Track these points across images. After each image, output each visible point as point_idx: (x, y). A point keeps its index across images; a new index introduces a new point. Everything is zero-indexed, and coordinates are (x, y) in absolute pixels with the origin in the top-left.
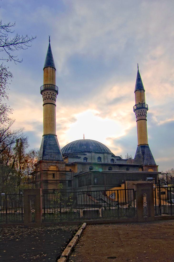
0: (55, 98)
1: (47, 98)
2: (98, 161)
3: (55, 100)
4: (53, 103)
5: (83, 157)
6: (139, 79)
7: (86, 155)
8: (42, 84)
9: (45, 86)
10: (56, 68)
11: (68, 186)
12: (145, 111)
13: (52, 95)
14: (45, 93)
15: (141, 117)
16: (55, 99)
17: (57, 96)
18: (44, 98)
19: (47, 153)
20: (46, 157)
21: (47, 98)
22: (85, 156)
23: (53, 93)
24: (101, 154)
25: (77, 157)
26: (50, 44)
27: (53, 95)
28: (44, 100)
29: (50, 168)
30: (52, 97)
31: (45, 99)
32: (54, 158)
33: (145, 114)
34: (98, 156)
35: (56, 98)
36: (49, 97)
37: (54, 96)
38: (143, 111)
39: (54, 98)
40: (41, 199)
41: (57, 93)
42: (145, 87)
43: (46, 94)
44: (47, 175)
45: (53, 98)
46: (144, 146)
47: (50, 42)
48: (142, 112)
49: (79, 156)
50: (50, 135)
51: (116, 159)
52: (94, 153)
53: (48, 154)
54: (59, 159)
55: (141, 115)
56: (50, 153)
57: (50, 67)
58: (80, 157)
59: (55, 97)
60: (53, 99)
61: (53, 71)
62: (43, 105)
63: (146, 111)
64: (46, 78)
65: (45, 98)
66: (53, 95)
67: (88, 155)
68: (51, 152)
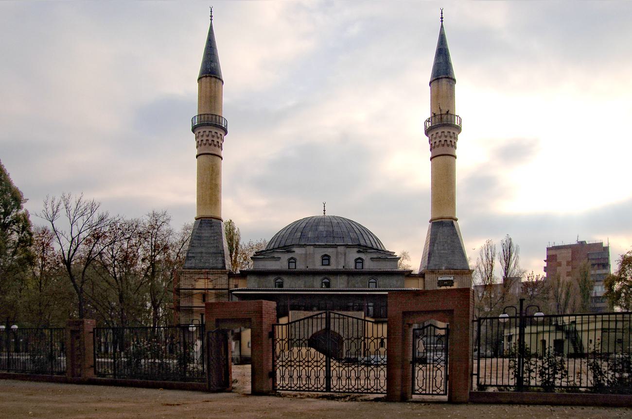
0: (220, 142)
1: (443, 142)
2: (323, 265)
3: (220, 147)
4: (216, 153)
5: (285, 257)
6: (442, 52)
7: (294, 252)
8: (428, 115)
9: (202, 117)
10: (223, 80)
11: (252, 319)
12: (452, 134)
13: (446, 137)
14: (199, 133)
15: (441, 148)
16: (220, 145)
17: (226, 138)
18: (198, 142)
19: (193, 255)
20: (190, 262)
21: (210, 142)
22: (291, 255)
23: (216, 133)
24: (329, 247)
25: (274, 257)
26: (442, 26)
27: (216, 136)
28: (197, 147)
29: (197, 283)
30: (446, 141)
31: (201, 145)
32: (206, 263)
33: (218, 142)
34: (322, 252)
35: (222, 142)
36: (208, 140)
37: (218, 138)
38: (446, 134)
39: (451, 141)
40: (469, 348)
41: (225, 131)
42: (457, 71)
43: (440, 134)
44: (191, 295)
45: (215, 143)
46: (439, 222)
47: (211, 20)
48: (446, 137)
49: (276, 255)
50: (203, 219)
51: (369, 257)
52: (312, 247)
53: (194, 257)
54: (215, 265)
55: (443, 142)
56: (200, 255)
57: (205, 78)
58: (280, 258)
59: (452, 140)
60: (215, 146)
61: (211, 83)
62: (197, 157)
63: (221, 135)
64: (436, 98)
65: (433, 146)
66: (216, 136)
67: (298, 251)
68: (202, 253)
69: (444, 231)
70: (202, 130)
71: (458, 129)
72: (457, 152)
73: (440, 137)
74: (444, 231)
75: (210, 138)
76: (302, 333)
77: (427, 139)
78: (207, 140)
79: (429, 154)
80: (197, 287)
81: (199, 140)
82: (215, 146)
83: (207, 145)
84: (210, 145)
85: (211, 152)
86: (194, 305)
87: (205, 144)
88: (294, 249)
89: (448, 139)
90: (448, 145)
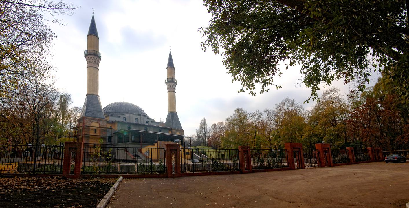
0: (98, 63)
25: (117, 116)
28: (87, 64)
29: (92, 124)
40: (125, 163)
43: (90, 58)
49: (119, 115)
55: (91, 62)
64: (90, 44)
68: (94, 110)
69: (92, 99)
70: (90, 57)
71: (176, 83)
72: (176, 91)
73: (90, 59)
74: (92, 99)
75: (172, 86)
76: (121, 153)
77: (86, 59)
78: (90, 61)
79: (86, 66)
80: (92, 126)
81: (89, 60)
82: (94, 63)
83: (90, 63)
84: (91, 63)
85: (92, 66)
86: (90, 134)
87: (91, 63)
88: (126, 114)
89: (173, 86)
90: (96, 64)
